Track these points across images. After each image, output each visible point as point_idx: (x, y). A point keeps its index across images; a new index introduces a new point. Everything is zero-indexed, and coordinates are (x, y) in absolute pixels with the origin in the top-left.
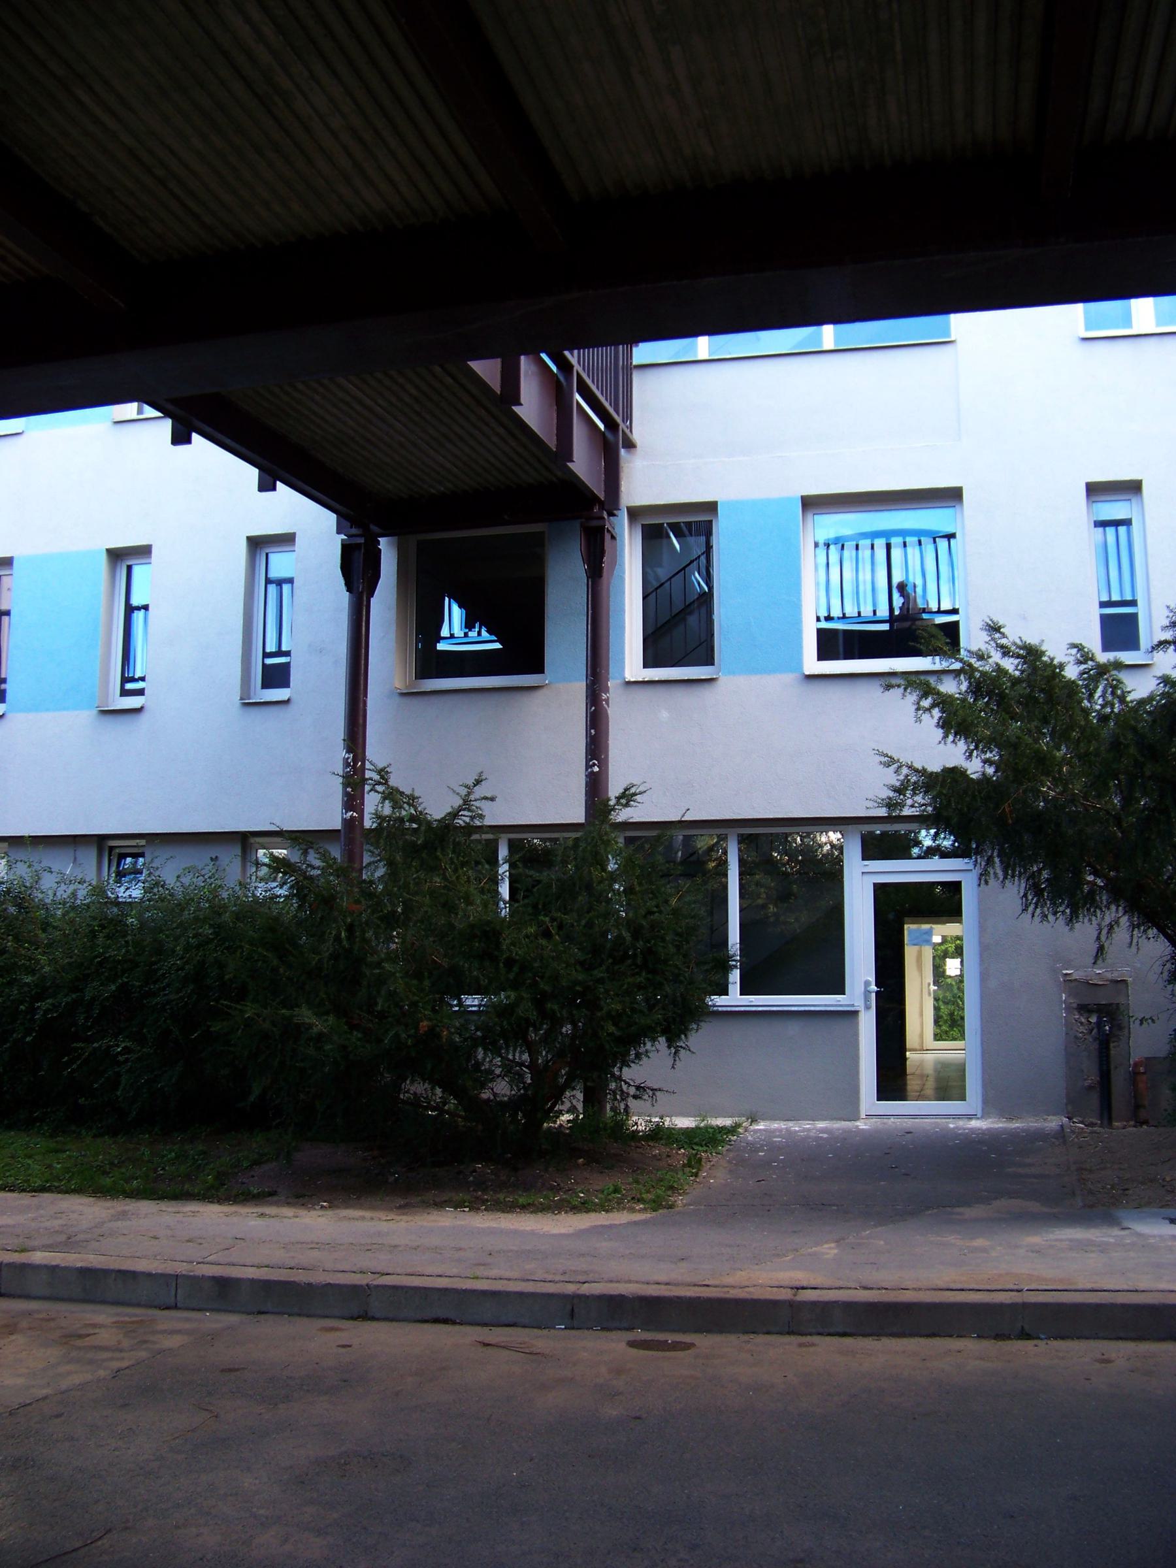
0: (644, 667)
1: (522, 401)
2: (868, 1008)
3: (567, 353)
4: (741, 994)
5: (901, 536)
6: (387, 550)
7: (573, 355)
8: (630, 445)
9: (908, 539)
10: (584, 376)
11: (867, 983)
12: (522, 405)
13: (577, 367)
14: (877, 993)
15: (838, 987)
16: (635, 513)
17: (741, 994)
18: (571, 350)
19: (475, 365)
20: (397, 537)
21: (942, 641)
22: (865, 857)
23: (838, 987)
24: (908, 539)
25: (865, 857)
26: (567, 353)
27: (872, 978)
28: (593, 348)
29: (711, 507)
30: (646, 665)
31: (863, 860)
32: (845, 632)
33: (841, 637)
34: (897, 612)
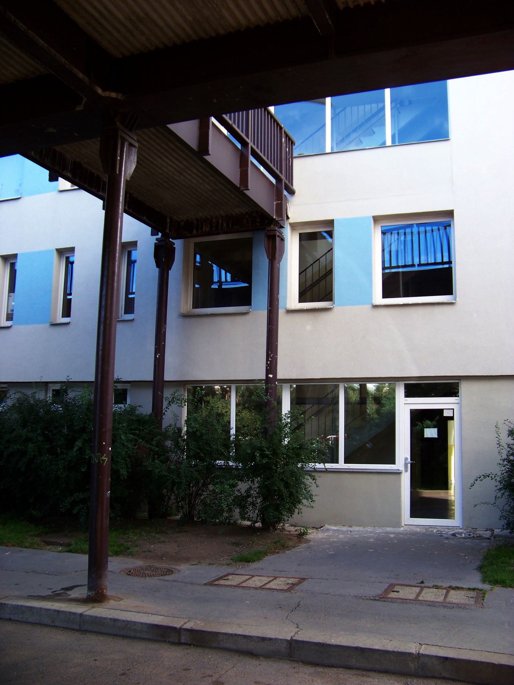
0: (299, 302)
1: (210, 153)
2: (406, 471)
3: (224, 116)
4: (345, 463)
5: (256, 528)
6: (178, 244)
7: (227, 116)
8: (292, 192)
9: (434, 228)
10: (255, 148)
11: (406, 459)
12: (210, 155)
13: (251, 144)
14: (411, 464)
15: (393, 462)
16: (294, 226)
17: (345, 463)
18: (226, 114)
19: (174, 127)
20: (183, 239)
21: (321, 246)
22: (406, 396)
23: (393, 462)
24: (434, 228)
25: (406, 396)
26: (224, 116)
27: (409, 457)
28: (238, 112)
29: (330, 223)
30: (300, 301)
31: (405, 397)
32: (403, 272)
33: (401, 274)
34: (133, 265)
